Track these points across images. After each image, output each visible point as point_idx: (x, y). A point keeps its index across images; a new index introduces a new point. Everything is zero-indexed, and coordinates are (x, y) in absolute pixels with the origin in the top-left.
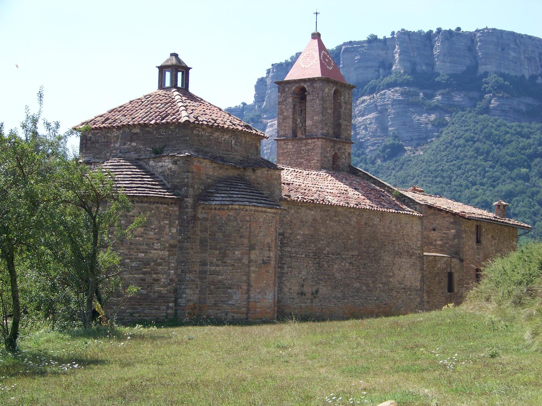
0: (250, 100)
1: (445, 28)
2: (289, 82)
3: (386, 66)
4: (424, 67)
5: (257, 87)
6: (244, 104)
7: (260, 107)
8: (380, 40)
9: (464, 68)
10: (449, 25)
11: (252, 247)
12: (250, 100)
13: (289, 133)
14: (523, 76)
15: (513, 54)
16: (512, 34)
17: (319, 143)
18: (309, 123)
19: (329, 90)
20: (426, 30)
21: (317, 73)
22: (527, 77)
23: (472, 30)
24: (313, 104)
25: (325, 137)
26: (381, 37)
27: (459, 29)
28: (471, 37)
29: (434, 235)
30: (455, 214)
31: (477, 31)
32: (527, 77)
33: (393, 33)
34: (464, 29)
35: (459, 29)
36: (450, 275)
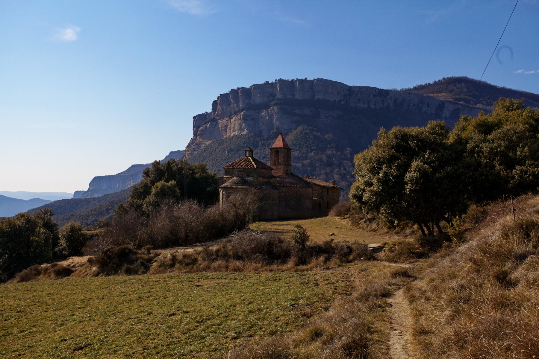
0: (209, 110)
1: (300, 78)
2: (273, 148)
3: (273, 95)
4: (290, 96)
5: (213, 105)
6: (207, 112)
7: (214, 114)
8: (270, 84)
9: (350, 222)
10: (302, 77)
11: (273, 200)
12: (209, 110)
13: (273, 163)
14: (335, 101)
15: (331, 90)
16: (330, 81)
17: (283, 166)
18: (279, 160)
19: (286, 151)
20: (291, 79)
21: (282, 146)
22: (337, 101)
23: (312, 79)
24: (281, 155)
25: (285, 165)
26: (270, 82)
27: (306, 78)
28: (312, 82)
29: (314, 192)
30: (321, 186)
31: (315, 79)
32: (337, 101)
33: (276, 80)
34: (308, 79)
35: (306, 78)
36: (320, 204)
